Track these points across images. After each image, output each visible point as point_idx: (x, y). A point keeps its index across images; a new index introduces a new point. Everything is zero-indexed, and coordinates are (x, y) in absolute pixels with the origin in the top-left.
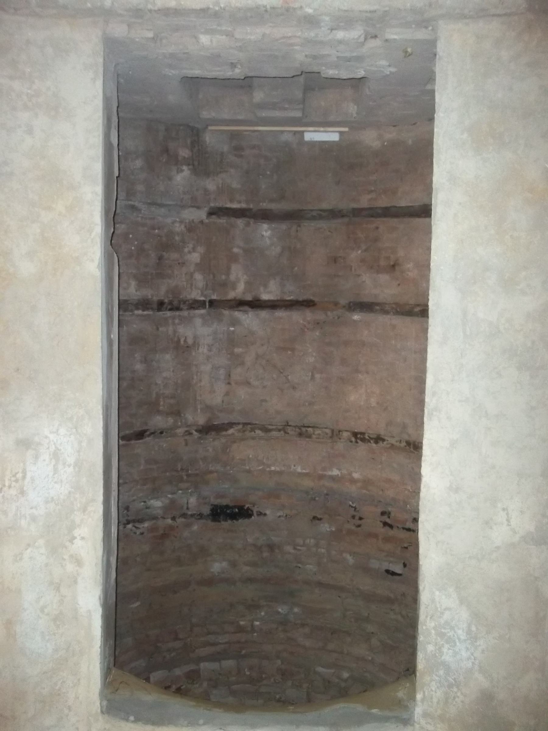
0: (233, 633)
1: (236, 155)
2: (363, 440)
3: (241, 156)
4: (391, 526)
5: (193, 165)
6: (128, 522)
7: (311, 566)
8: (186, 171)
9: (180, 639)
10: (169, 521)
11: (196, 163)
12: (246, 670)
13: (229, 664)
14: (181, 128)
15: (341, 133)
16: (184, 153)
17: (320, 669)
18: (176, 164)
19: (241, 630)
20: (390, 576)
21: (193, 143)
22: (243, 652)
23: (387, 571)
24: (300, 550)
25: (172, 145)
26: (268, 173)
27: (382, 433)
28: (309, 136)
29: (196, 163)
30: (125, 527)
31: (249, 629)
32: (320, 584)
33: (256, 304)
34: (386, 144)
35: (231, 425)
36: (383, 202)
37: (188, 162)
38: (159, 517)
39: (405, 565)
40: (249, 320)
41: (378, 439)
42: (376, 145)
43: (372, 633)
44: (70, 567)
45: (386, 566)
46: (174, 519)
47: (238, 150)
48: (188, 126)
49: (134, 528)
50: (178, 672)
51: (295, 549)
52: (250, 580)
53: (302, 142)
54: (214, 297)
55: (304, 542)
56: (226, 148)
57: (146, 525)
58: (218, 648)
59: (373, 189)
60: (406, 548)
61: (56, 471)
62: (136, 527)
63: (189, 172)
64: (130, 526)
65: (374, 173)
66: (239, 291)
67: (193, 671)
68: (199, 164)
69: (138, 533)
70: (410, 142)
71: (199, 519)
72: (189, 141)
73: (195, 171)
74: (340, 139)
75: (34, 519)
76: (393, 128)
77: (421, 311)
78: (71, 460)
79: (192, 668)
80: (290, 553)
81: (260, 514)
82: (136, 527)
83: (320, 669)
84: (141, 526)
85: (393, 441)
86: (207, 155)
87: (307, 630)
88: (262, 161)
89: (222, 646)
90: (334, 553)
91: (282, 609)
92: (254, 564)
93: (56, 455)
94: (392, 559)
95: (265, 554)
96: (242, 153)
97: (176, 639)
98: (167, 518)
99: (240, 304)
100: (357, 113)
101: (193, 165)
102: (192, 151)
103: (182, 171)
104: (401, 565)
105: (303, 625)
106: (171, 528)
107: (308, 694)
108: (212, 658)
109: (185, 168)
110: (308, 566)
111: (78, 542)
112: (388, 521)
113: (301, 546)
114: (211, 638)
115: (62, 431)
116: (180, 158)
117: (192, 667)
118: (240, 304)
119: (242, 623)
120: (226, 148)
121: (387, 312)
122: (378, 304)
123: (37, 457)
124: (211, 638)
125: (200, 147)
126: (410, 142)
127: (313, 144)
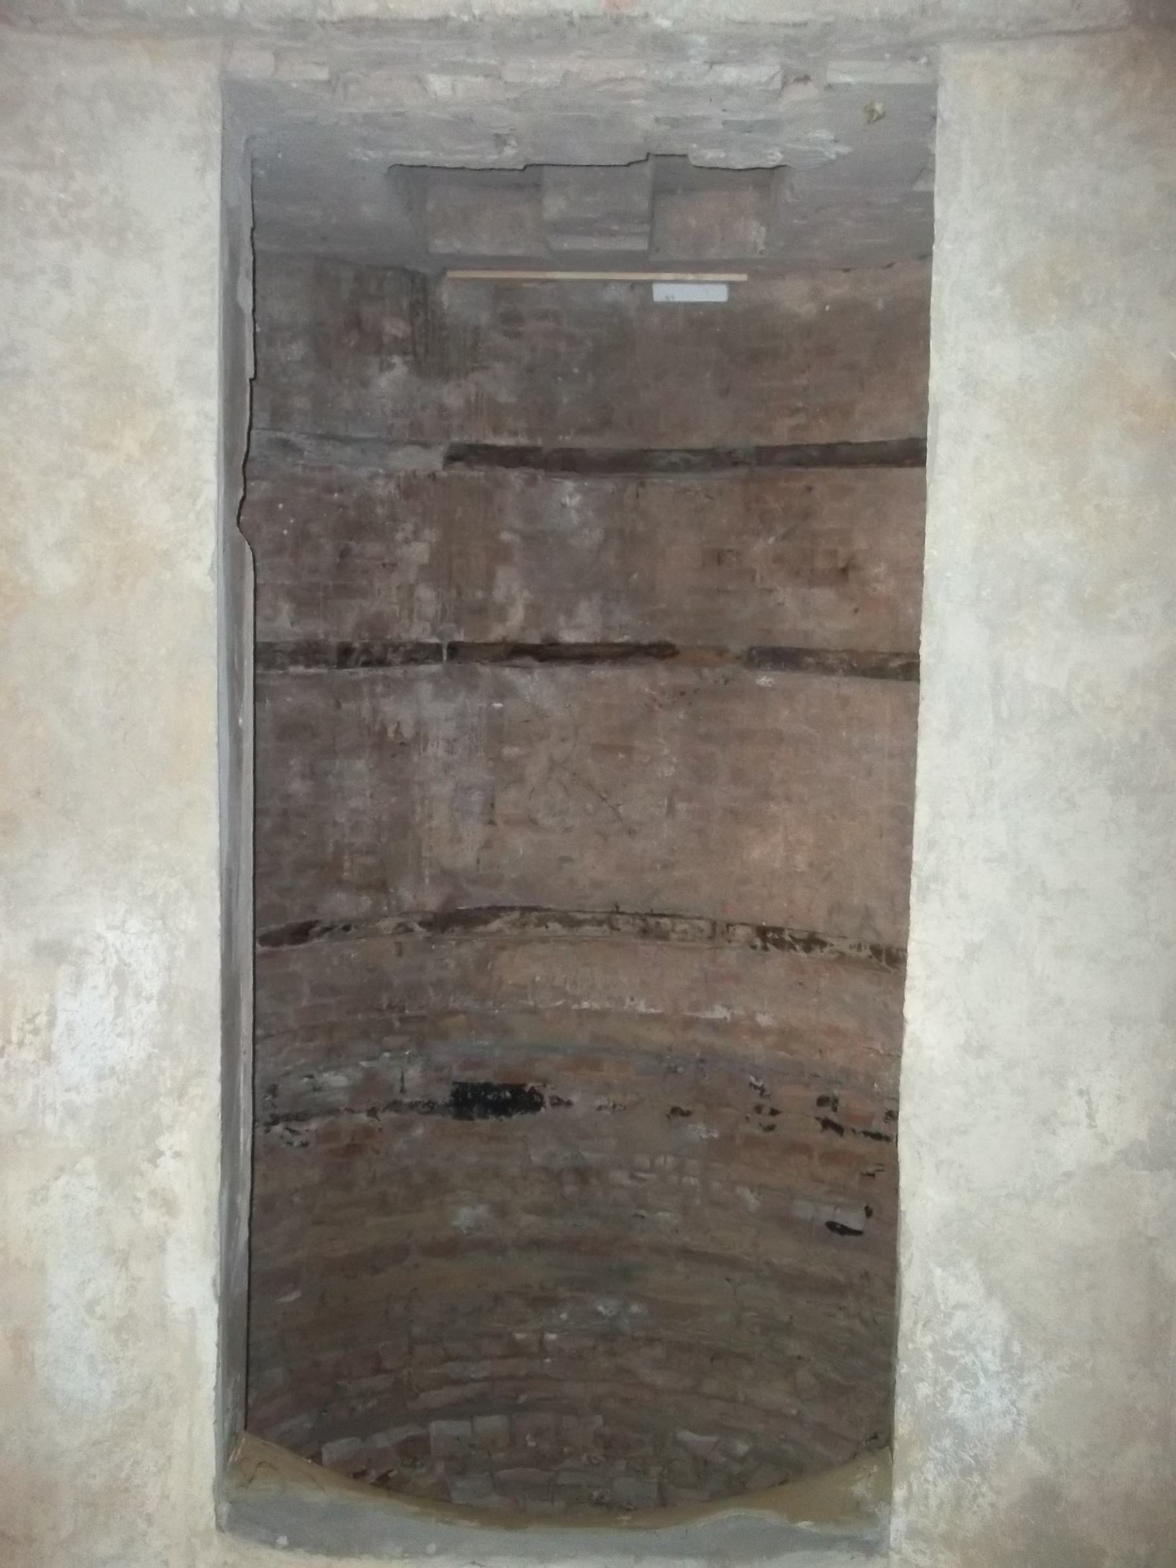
0: (499, 1358)
1: (506, 334)
2: (780, 944)
3: (518, 335)
4: (839, 1129)
5: (415, 354)
6: (275, 1120)
7: (668, 1215)
8: (400, 368)
9: (386, 1371)
10: (363, 1118)
11: (421, 350)
12: (528, 1437)
13: (492, 1423)
14: (389, 274)
15: (732, 285)
16: (395, 328)
17: (686, 1436)
18: (378, 352)
19: (517, 1351)
20: (837, 1236)
21: (413, 306)
22: (522, 1398)
23: (831, 1226)
24: (643, 1180)
25: (368, 312)
26: (576, 370)
27: (820, 928)
28: (663, 293)
29: (421, 350)
30: (268, 1131)
31: (535, 1349)
32: (686, 1253)
33: (549, 653)
34: (827, 308)
35: (496, 911)
36: (822, 434)
37: (402, 347)
38: (342, 1108)
39: (869, 1213)
40: (535, 686)
41: (812, 942)
42: (807, 310)
43: (799, 1358)
44: (150, 1217)
45: (827, 1213)
46: (372, 1112)
47: (511, 321)
48: (405, 271)
49: (287, 1133)
50: (382, 1441)
51: (633, 1177)
52: (537, 1244)
53: (647, 305)
54: (460, 637)
55: (652, 1162)
56: (484, 318)
57: (314, 1125)
58: (469, 1391)
59: (800, 405)
60: (872, 1175)
61: (119, 1009)
62: (292, 1131)
63: (405, 369)
64: (278, 1129)
65: (803, 372)
66: (513, 624)
67: (413, 1439)
68: (427, 351)
69: (296, 1144)
70: (880, 305)
71: (427, 1113)
72: (405, 303)
73: (419, 368)
74: (730, 299)
75: (72, 1113)
76: (843, 275)
77: (903, 668)
78: (152, 987)
79: (411, 1433)
80: (622, 1187)
81: (558, 1102)
82: (292, 1131)
83: (686, 1436)
84: (301, 1128)
85: (843, 946)
86: (444, 333)
87: (658, 1351)
88: (562, 346)
89: (477, 1386)
90: (716, 1185)
91: (605, 1307)
92: (545, 1211)
93: (120, 977)
94: (840, 1199)
95: (569, 1189)
96: (520, 329)
97: (378, 1370)
98: (360, 1112)
99: (515, 652)
100: (766, 243)
101: (415, 354)
102: (412, 325)
103: (391, 366)
104: (861, 1213)
105: (650, 1341)
106: (368, 1132)
107: (661, 1488)
108: (455, 1411)
109: (396, 359)
110: (660, 1214)
111: (168, 1163)
112: (833, 1117)
113: (646, 1171)
114: (454, 1369)
115: (134, 924)
116: (386, 340)
117: (413, 1430)
118: (515, 652)
119: (519, 1336)
120: (484, 318)
121: (829, 670)
122: (810, 652)
123: (78, 981)
124: (454, 1369)
125: (429, 316)
126: (880, 305)
127: (670, 309)
